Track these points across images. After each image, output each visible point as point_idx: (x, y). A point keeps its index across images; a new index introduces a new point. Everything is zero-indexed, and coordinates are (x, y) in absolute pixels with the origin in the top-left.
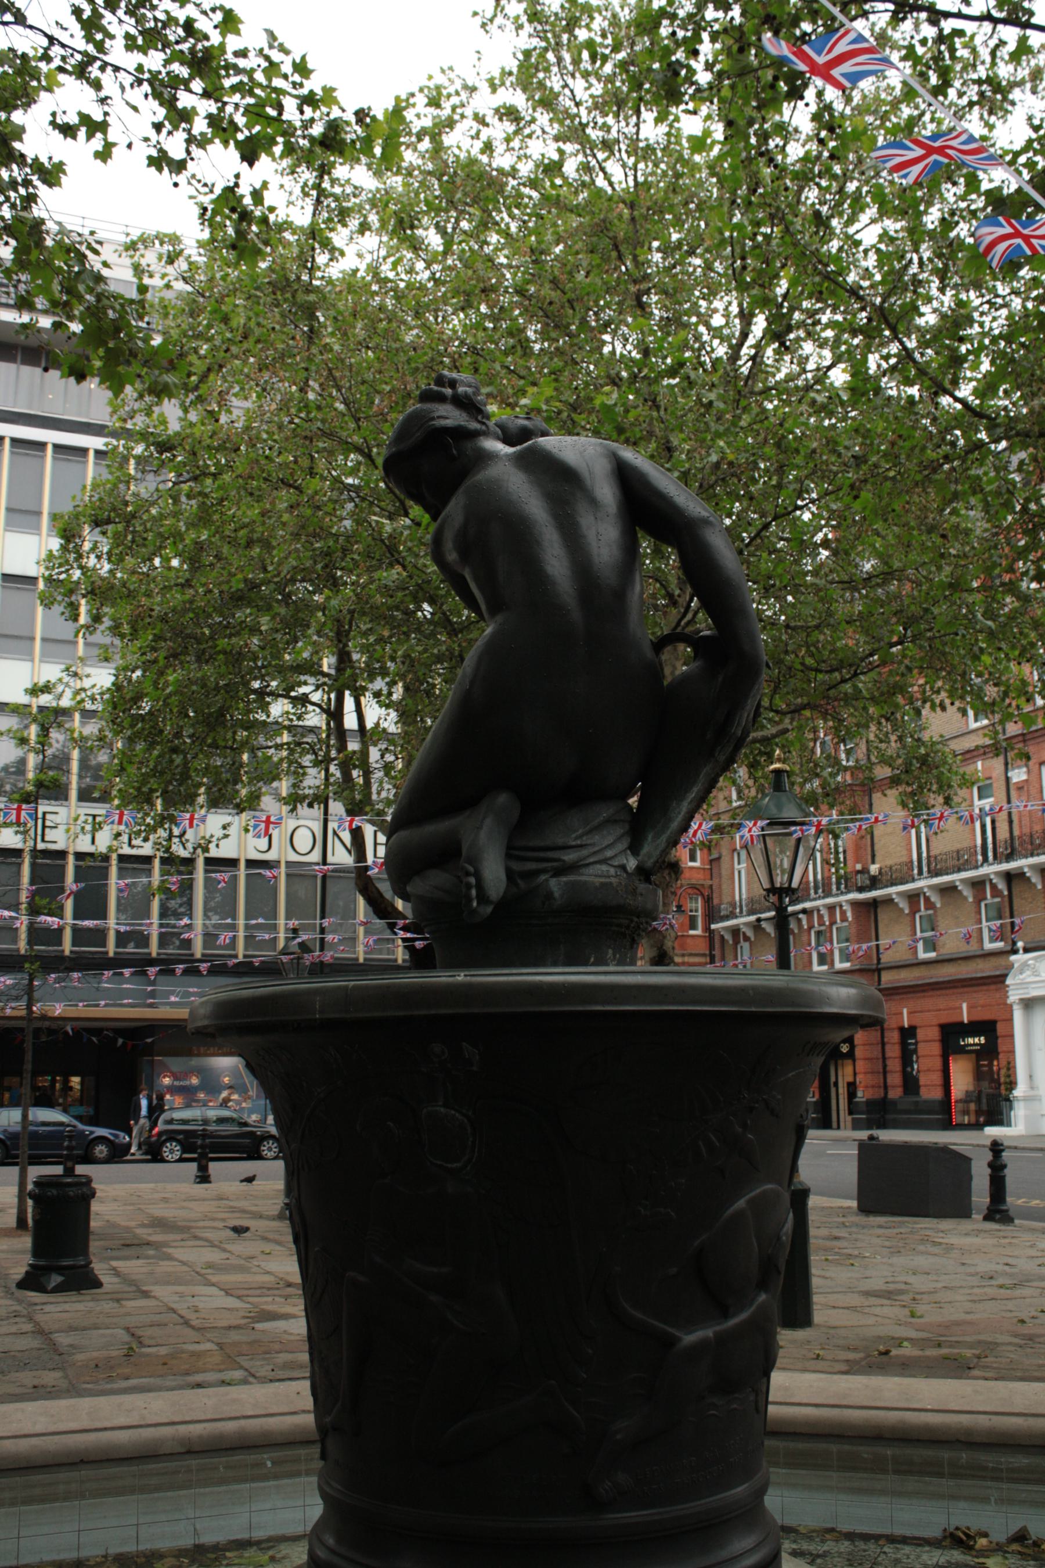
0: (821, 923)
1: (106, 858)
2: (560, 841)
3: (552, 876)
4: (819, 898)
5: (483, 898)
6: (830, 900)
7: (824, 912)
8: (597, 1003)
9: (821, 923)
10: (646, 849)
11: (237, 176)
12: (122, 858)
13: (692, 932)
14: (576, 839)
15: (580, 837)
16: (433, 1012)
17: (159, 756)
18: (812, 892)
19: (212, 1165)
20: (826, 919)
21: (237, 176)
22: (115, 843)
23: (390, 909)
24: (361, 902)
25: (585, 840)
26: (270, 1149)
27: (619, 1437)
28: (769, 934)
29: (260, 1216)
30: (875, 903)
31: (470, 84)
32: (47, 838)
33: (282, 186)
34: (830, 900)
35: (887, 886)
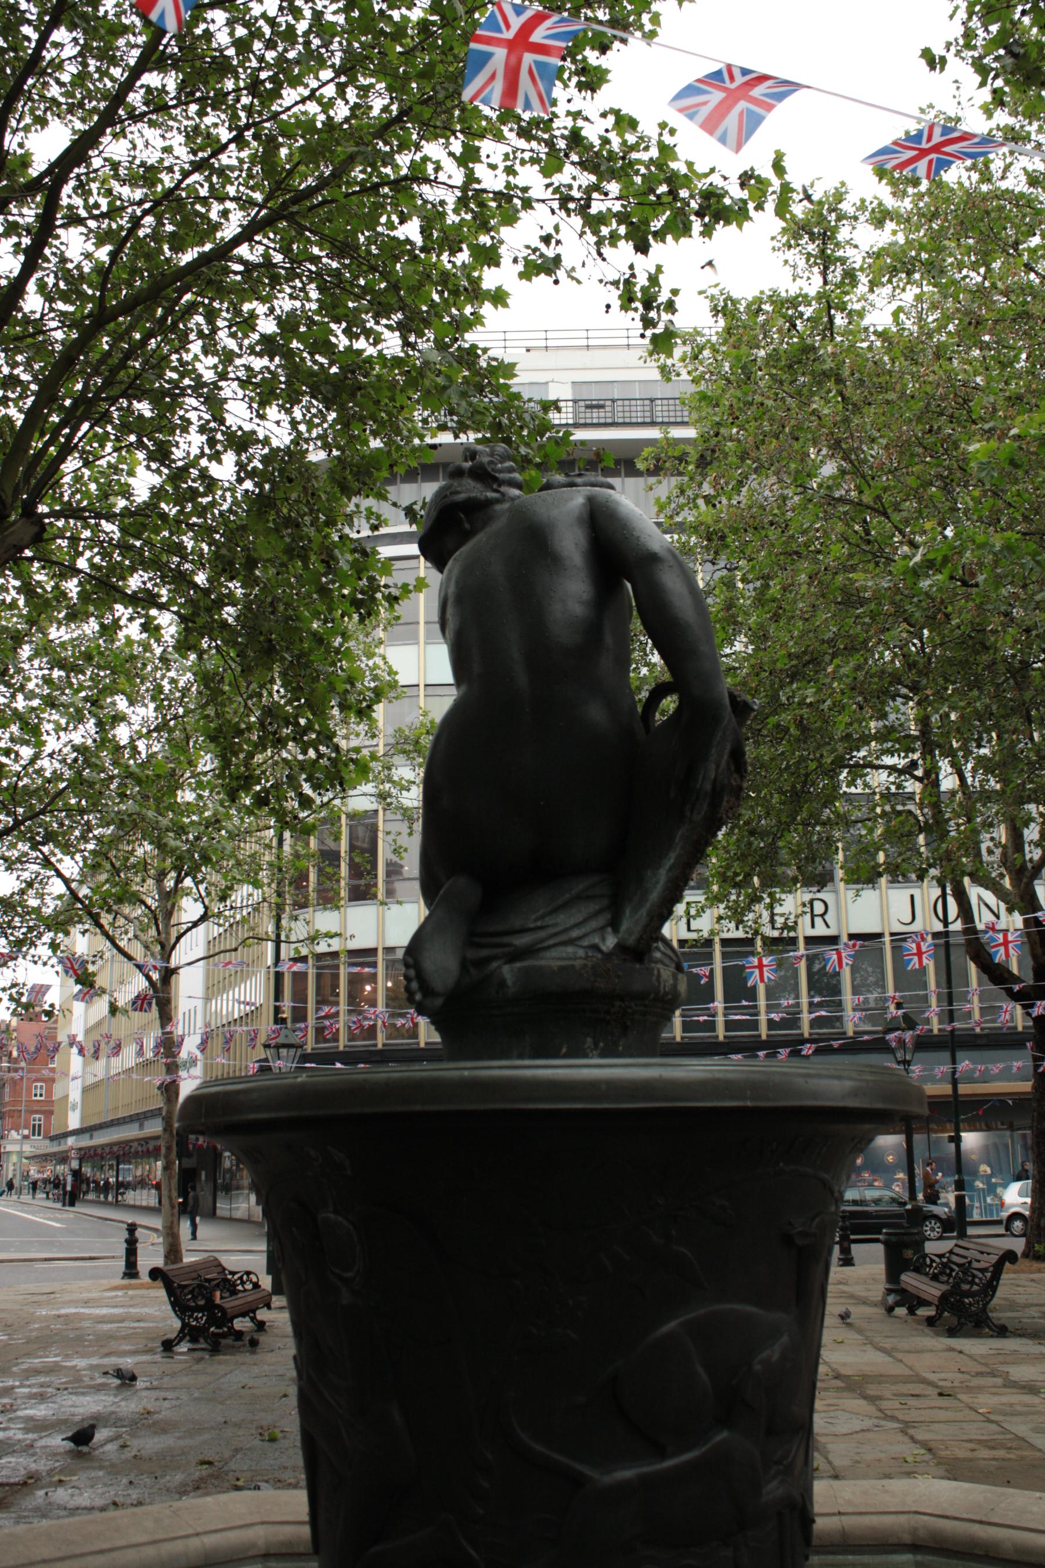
1: (709, 943)
2: (517, 923)
3: (506, 963)
10: (624, 927)
11: (631, 267)
12: (725, 942)
14: (536, 920)
15: (542, 917)
17: (738, 840)
19: (854, 1247)
21: (631, 267)
22: (717, 926)
23: (1006, 975)
24: (972, 968)
25: (549, 921)
26: (933, 1229)
29: (864, 1302)
31: (953, 116)
32: (692, 928)
33: (786, 262)
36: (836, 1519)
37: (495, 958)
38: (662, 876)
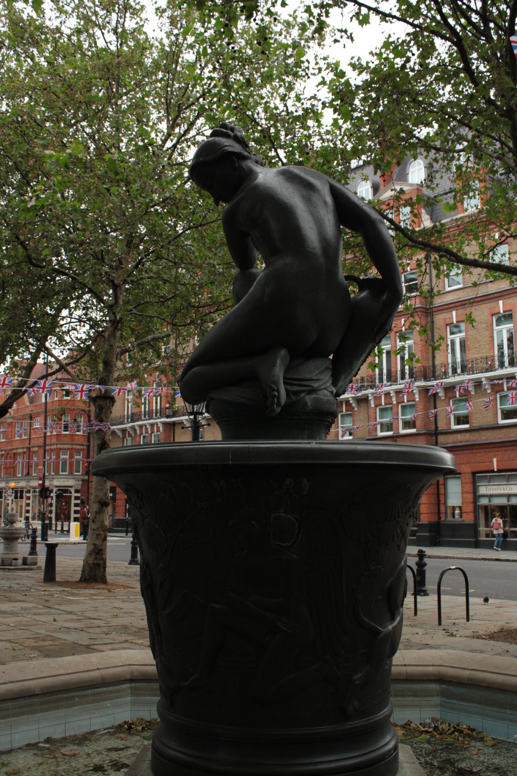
0: (147, 432)
2: (309, 376)
3: (307, 394)
4: (146, 420)
5: (279, 404)
6: (152, 421)
7: (148, 427)
8: (381, 460)
9: (147, 432)
13: (77, 433)
16: (302, 462)
18: (143, 416)
20: (149, 430)
27: (357, 682)
28: (119, 436)
30: (174, 424)
34: (152, 421)
35: (181, 416)
36: (97, 672)
37: (303, 391)
38: (365, 355)
